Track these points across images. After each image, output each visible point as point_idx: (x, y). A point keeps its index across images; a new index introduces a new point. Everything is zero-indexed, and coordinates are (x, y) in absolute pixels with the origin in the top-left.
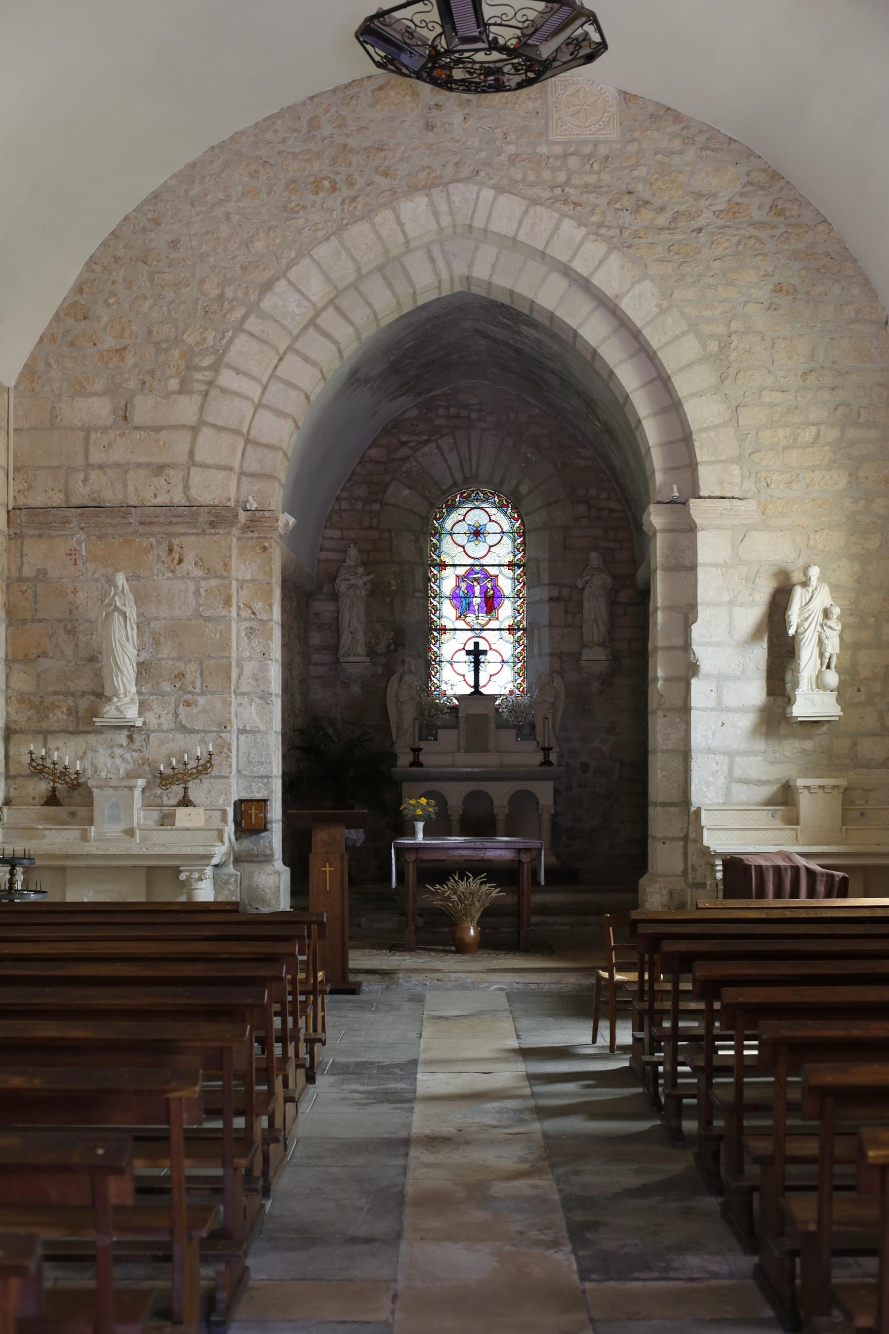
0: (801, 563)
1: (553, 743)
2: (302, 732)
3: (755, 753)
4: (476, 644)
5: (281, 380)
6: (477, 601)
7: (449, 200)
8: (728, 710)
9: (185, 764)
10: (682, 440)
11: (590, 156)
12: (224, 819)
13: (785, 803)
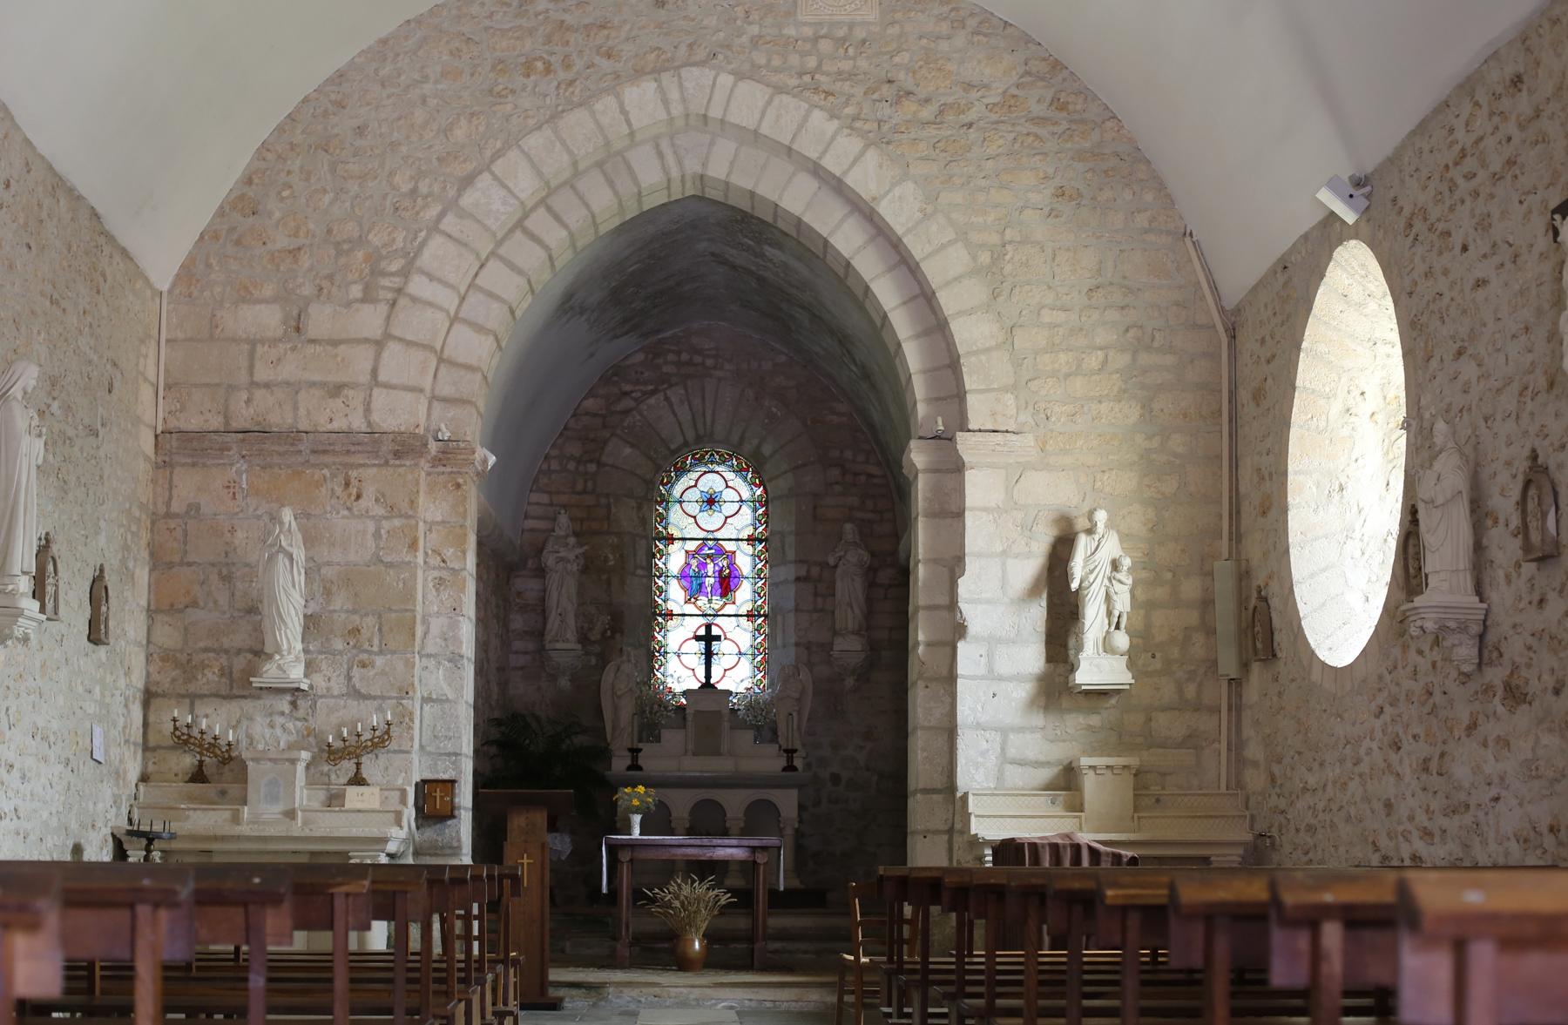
0: (1086, 508)
1: (798, 745)
2: (498, 722)
3: (1033, 730)
4: (708, 627)
5: (481, 290)
6: (710, 581)
7: (681, 86)
8: (1001, 678)
9: (359, 735)
10: (948, 367)
11: (844, 39)
12: (403, 801)
13: (1067, 788)
